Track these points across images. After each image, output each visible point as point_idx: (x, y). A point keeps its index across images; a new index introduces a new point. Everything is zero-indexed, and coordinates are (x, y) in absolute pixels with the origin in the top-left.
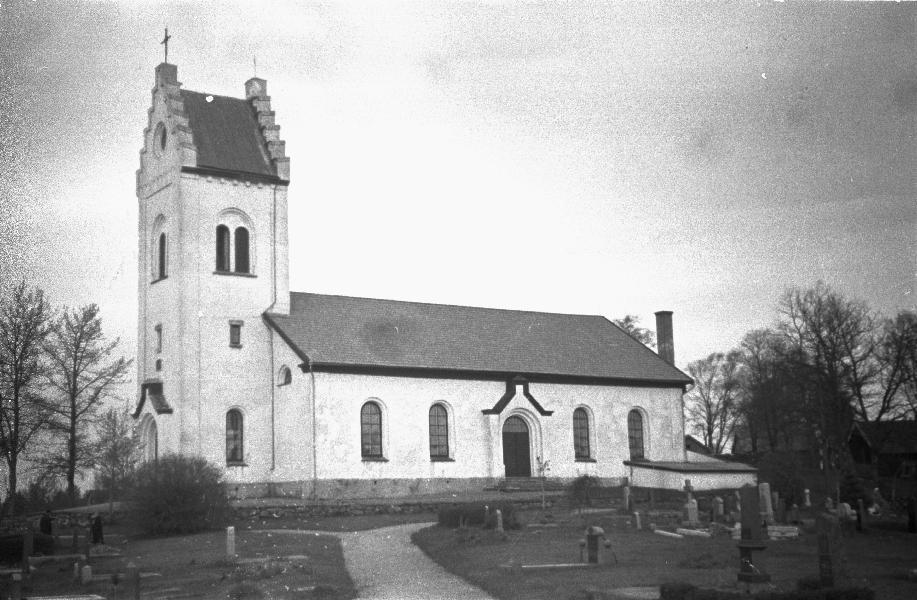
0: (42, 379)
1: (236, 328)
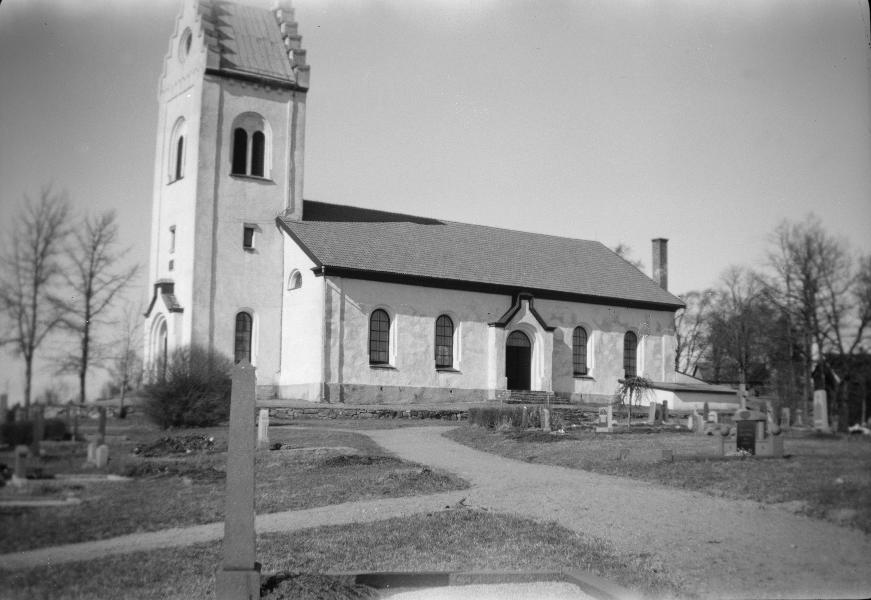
0: (59, 279)
1: (249, 232)
